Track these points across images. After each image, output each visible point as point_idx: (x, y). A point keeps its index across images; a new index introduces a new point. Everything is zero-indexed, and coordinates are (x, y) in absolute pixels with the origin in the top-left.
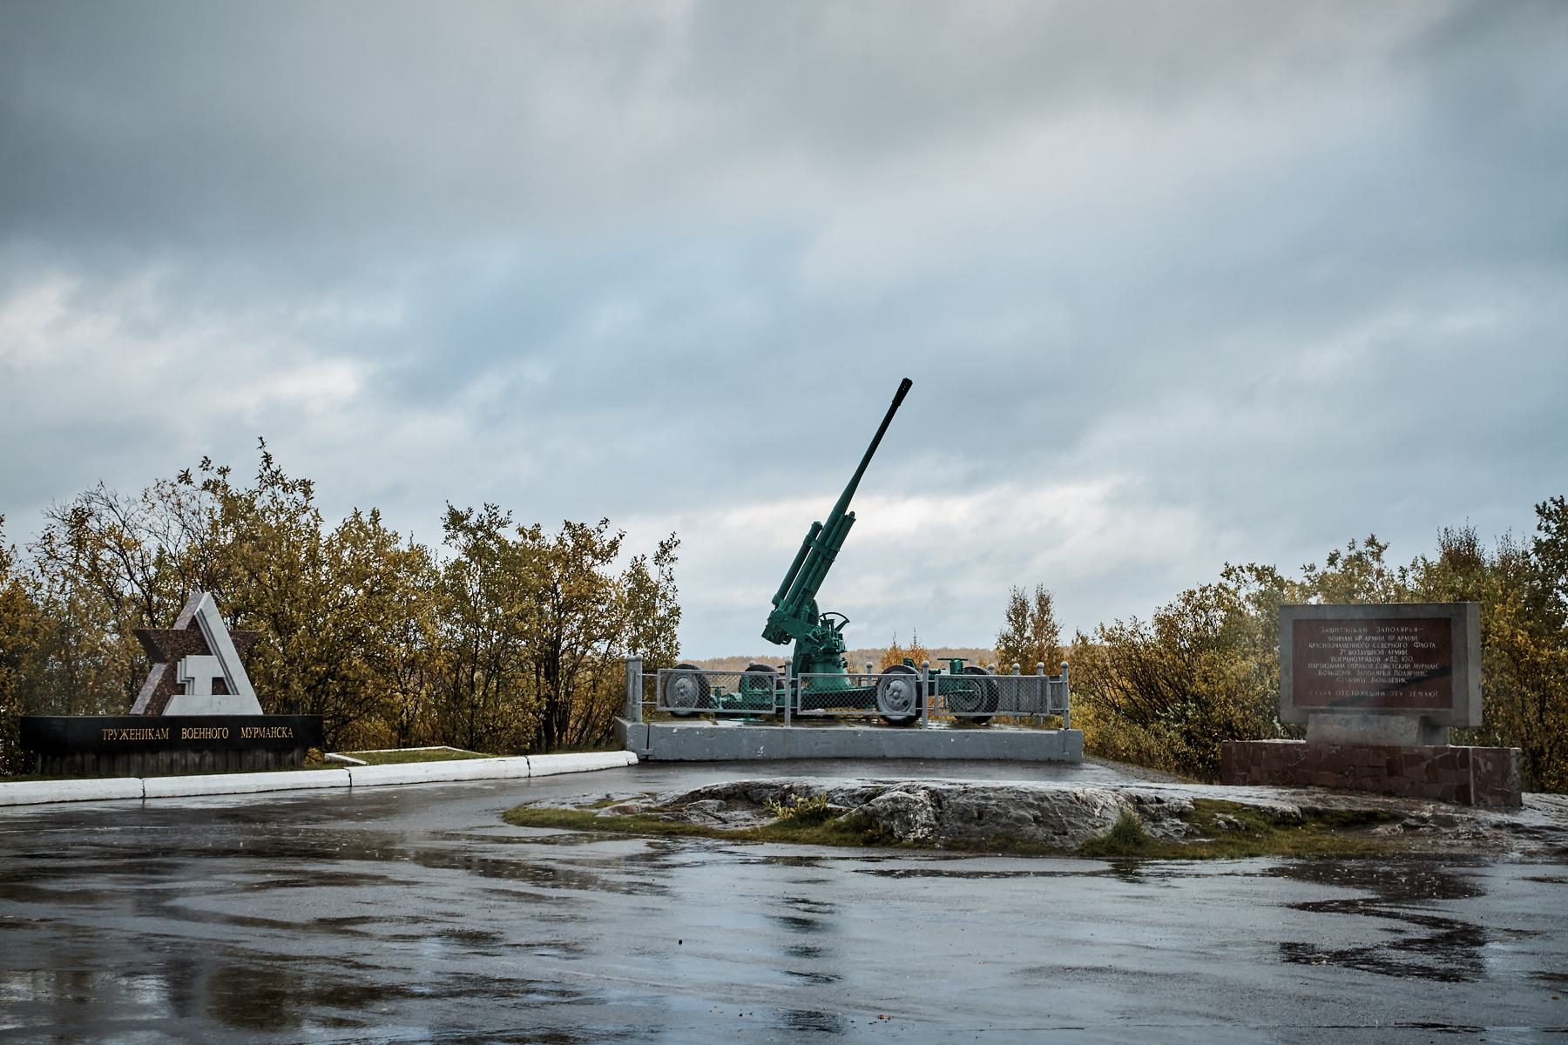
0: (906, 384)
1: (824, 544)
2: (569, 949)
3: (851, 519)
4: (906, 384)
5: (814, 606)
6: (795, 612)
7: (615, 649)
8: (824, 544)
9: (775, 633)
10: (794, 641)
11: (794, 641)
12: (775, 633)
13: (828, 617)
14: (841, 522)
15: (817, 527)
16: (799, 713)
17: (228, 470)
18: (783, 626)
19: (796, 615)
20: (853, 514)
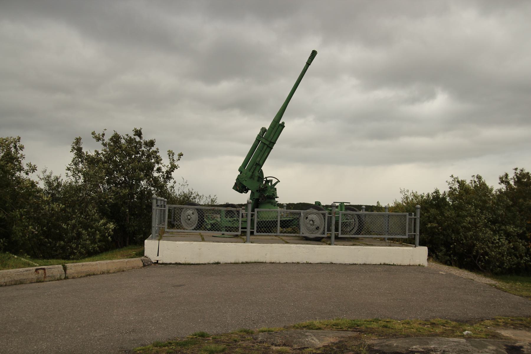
0: (314, 53)
1: (266, 142)
2: (252, 233)
3: (283, 126)
4: (314, 53)
5: (262, 172)
6: (251, 178)
7: (314, 322)
8: (266, 142)
9: (240, 187)
10: (250, 192)
11: (250, 192)
12: (240, 187)
13: (268, 179)
14: (277, 127)
15: (263, 130)
16: (340, 236)
17: (182, 155)
18: (244, 183)
19: (252, 177)
20: (283, 123)
